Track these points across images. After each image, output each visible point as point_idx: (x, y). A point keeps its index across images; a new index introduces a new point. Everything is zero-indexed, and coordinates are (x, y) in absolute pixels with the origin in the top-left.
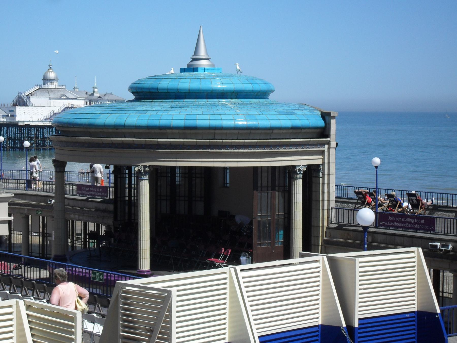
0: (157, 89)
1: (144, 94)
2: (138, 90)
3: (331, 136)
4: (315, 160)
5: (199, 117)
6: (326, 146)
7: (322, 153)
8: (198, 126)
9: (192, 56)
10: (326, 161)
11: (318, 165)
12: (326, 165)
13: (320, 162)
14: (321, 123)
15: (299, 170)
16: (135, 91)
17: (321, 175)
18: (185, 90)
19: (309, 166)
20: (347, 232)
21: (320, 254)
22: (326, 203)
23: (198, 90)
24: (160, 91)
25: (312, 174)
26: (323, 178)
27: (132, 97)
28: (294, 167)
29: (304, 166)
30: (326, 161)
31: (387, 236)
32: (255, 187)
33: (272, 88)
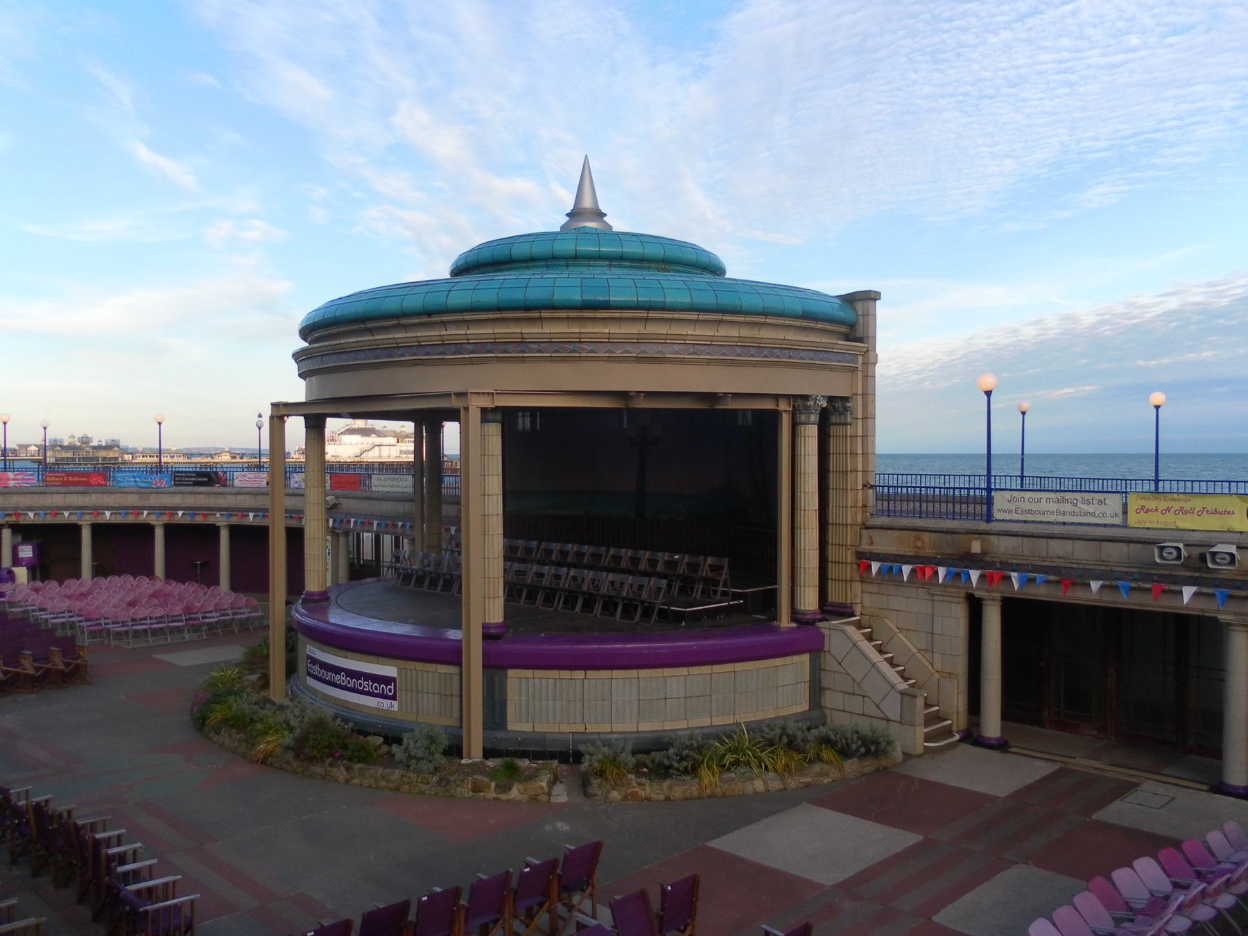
4: (836, 385)
11: (845, 399)
20: (914, 534)
28: (805, 398)
31: (1026, 540)
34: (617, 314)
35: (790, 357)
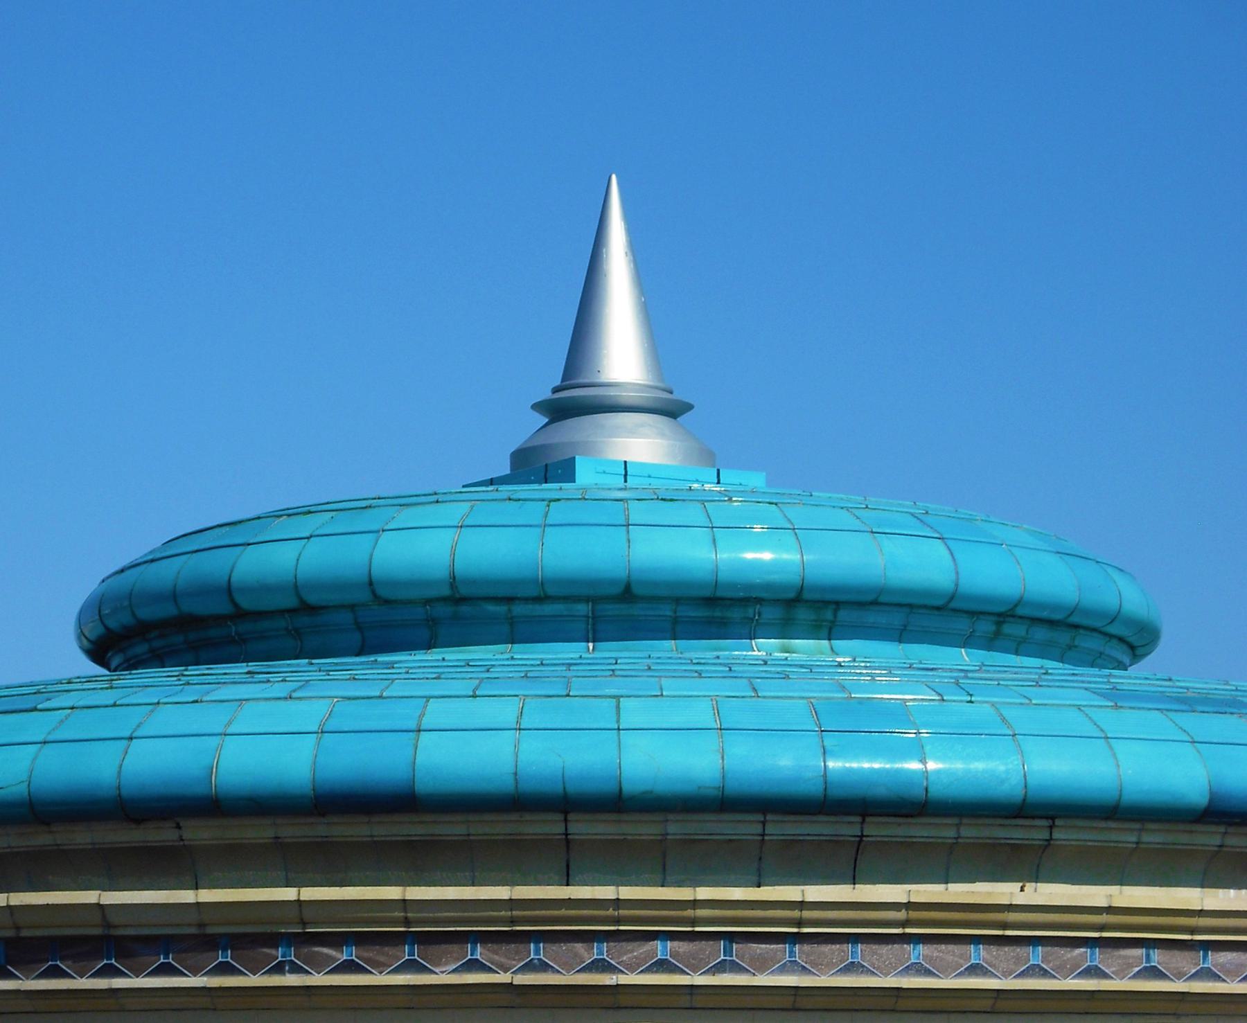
0: (228, 590)
5: (437, 713)
9: (545, 394)
24: (246, 603)
34: (452, 828)
35: (1154, 973)
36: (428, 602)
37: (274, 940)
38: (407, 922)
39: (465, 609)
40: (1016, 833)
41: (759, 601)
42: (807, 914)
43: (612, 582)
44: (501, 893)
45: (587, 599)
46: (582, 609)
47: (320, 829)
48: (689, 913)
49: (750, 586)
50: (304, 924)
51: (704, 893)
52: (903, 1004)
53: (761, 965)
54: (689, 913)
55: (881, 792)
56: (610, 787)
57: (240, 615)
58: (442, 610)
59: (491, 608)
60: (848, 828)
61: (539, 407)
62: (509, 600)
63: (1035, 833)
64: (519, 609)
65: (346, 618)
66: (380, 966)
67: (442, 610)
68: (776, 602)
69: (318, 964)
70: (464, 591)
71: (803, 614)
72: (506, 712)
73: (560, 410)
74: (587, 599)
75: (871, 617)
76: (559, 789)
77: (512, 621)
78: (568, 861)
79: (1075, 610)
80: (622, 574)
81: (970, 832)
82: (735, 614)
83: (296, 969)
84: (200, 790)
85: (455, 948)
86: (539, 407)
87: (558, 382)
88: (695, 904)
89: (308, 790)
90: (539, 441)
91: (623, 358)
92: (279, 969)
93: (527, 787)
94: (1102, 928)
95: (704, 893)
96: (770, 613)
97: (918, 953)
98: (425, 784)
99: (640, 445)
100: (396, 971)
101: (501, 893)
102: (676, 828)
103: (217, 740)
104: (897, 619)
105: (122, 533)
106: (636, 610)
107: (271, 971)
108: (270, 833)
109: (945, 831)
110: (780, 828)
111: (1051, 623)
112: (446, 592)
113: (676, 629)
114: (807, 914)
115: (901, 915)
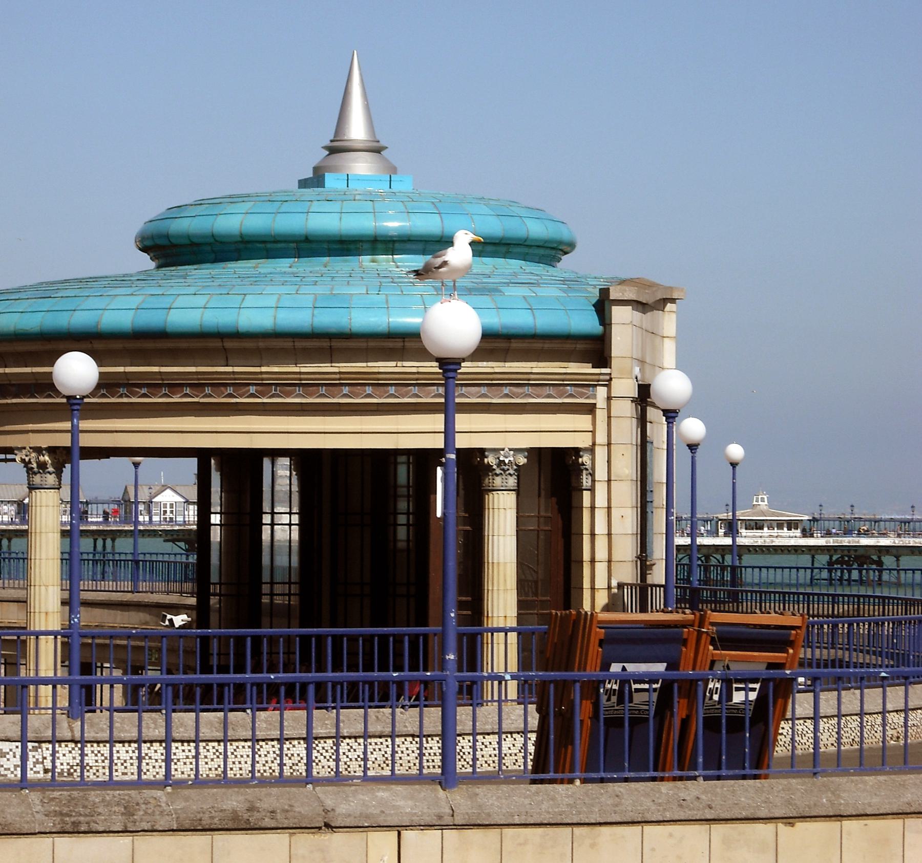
0: (167, 236)
1: (170, 250)
2: (159, 242)
3: (614, 362)
6: (602, 392)
7: (590, 409)
8: (169, 330)
9: (327, 143)
10: (601, 438)
11: (577, 451)
12: (601, 453)
13: (582, 441)
14: (588, 323)
15: (501, 463)
16: (148, 243)
17: (586, 481)
18: (230, 236)
19: (536, 454)
21: (652, 774)
22: (601, 568)
23: (203, 236)
24: (174, 241)
25: (556, 478)
26: (592, 490)
27: (146, 262)
28: (482, 452)
29: (517, 451)
30: (601, 438)
32: (665, 587)
33: (563, 233)
34: (183, 344)
36: (236, 242)
37: (119, 385)
38: (163, 380)
39: (249, 246)
40: (390, 344)
41: (361, 241)
42: (302, 376)
43: (300, 236)
44: (193, 369)
45: (293, 242)
46: (292, 245)
47: (138, 344)
48: (260, 376)
49: (354, 236)
50: (128, 380)
51: (264, 369)
52: (342, 408)
53: (288, 395)
54: (260, 376)
55: (333, 330)
56: (234, 330)
57: (174, 246)
58: (241, 246)
59: (258, 245)
60: (325, 344)
61: (326, 148)
62: (264, 242)
63: (399, 344)
64: (269, 246)
65: (208, 248)
66: (155, 395)
67: (241, 246)
68: (368, 241)
69: (134, 394)
70: (247, 239)
71: (380, 246)
72: (201, 301)
73: (335, 149)
74: (293, 242)
75: (408, 246)
76: (216, 330)
77: (267, 250)
78: (226, 357)
79: (502, 239)
80: (303, 232)
81: (372, 344)
82: (352, 246)
83: (127, 396)
84: (94, 330)
85: (179, 389)
86: (326, 148)
87: (332, 138)
88: (261, 373)
89: (130, 330)
90: (323, 165)
91: (357, 130)
92: (121, 396)
93: (205, 330)
94: (417, 380)
95: (264, 369)
96: (366, 246)
97: (346, 390)
98: (169, 329)
99: (361, 166)
100: (160, 397)
101: (193, 369)
102: (262, 344)
103: (101, 312)
104: (420, 246)
105: (145, 210)
106: (314, 246)
107: (119, 397)
108: (121, 346)
109: (362, 344)
110: (300, 344)
111: (494, 244)
112: (239, 239)
113: (330, 253)
114: (302, 376)
115: (338, 376)
